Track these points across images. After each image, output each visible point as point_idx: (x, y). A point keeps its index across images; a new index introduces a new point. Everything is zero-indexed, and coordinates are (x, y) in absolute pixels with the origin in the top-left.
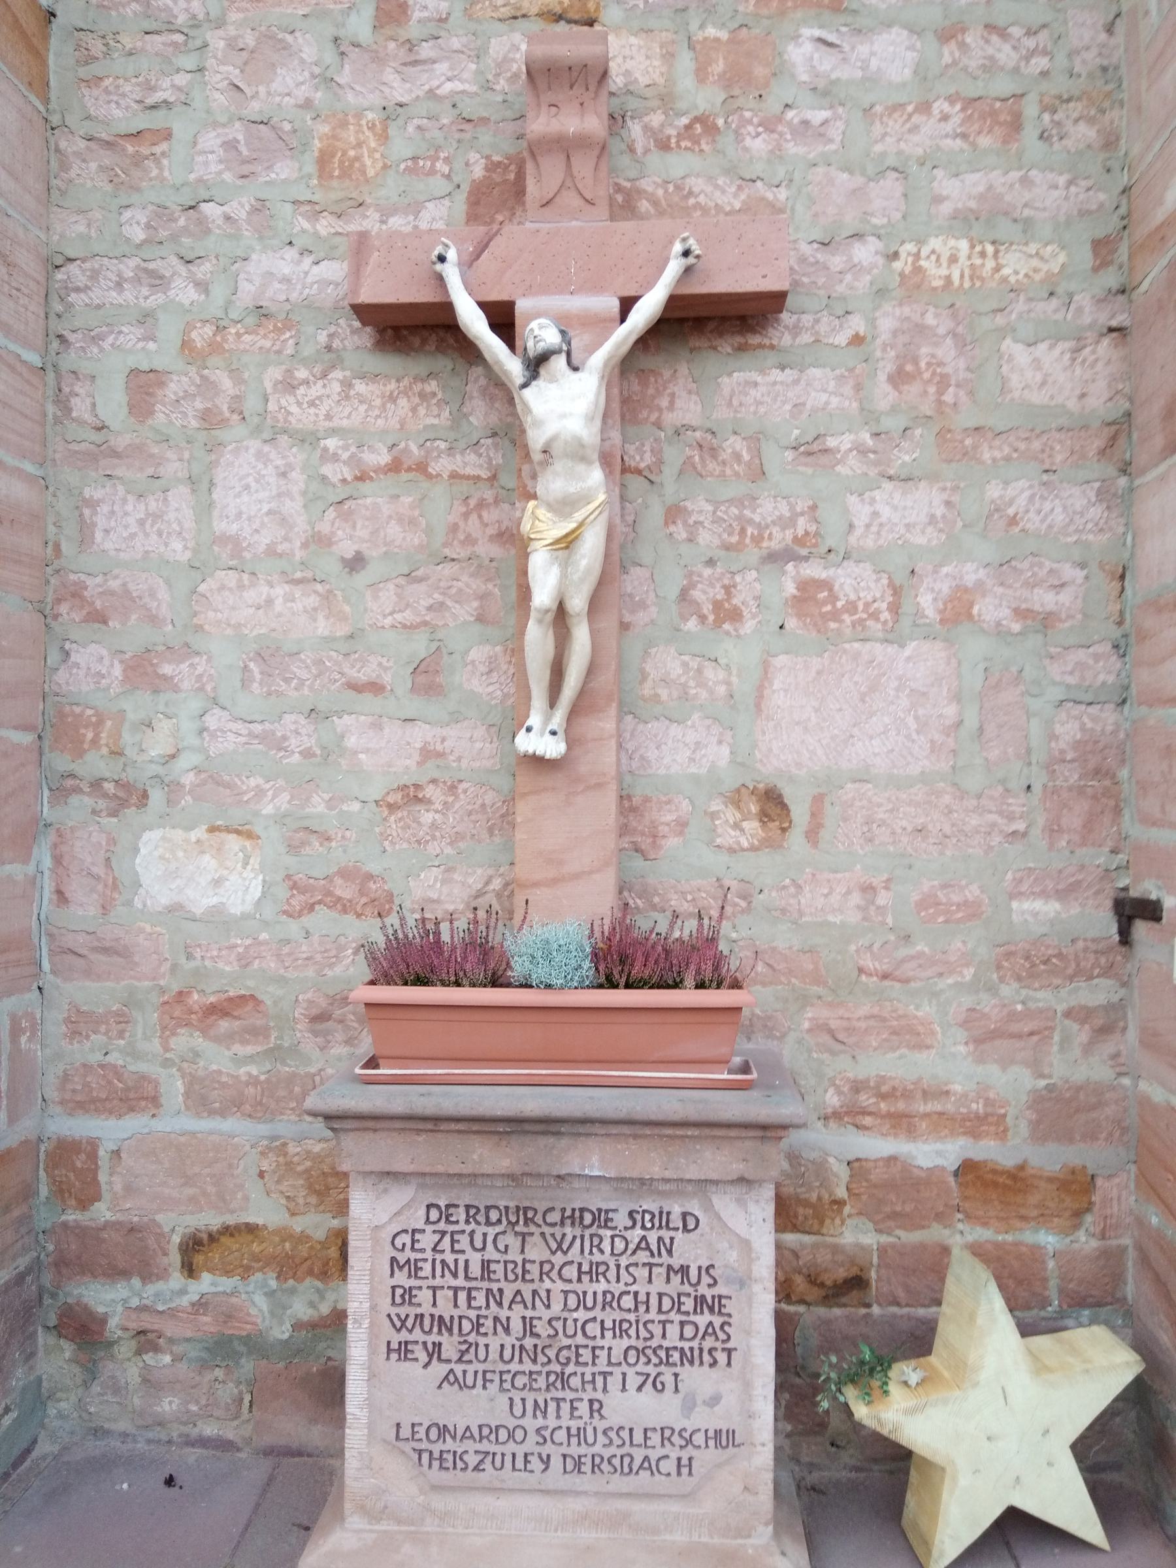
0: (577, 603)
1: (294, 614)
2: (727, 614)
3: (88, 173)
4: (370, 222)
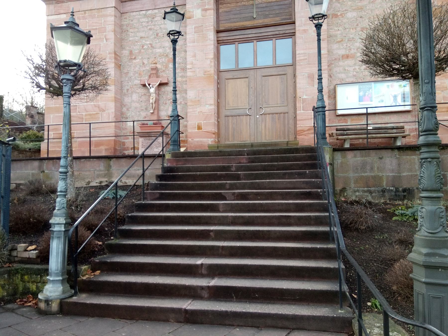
0: (153, 102)
1: (138, 105)
2: (166, 104)
3: (124, 75)
4: (142, 78)
